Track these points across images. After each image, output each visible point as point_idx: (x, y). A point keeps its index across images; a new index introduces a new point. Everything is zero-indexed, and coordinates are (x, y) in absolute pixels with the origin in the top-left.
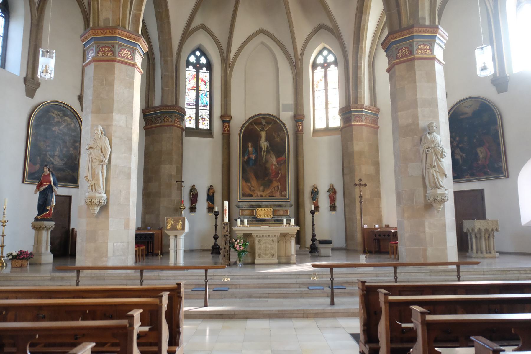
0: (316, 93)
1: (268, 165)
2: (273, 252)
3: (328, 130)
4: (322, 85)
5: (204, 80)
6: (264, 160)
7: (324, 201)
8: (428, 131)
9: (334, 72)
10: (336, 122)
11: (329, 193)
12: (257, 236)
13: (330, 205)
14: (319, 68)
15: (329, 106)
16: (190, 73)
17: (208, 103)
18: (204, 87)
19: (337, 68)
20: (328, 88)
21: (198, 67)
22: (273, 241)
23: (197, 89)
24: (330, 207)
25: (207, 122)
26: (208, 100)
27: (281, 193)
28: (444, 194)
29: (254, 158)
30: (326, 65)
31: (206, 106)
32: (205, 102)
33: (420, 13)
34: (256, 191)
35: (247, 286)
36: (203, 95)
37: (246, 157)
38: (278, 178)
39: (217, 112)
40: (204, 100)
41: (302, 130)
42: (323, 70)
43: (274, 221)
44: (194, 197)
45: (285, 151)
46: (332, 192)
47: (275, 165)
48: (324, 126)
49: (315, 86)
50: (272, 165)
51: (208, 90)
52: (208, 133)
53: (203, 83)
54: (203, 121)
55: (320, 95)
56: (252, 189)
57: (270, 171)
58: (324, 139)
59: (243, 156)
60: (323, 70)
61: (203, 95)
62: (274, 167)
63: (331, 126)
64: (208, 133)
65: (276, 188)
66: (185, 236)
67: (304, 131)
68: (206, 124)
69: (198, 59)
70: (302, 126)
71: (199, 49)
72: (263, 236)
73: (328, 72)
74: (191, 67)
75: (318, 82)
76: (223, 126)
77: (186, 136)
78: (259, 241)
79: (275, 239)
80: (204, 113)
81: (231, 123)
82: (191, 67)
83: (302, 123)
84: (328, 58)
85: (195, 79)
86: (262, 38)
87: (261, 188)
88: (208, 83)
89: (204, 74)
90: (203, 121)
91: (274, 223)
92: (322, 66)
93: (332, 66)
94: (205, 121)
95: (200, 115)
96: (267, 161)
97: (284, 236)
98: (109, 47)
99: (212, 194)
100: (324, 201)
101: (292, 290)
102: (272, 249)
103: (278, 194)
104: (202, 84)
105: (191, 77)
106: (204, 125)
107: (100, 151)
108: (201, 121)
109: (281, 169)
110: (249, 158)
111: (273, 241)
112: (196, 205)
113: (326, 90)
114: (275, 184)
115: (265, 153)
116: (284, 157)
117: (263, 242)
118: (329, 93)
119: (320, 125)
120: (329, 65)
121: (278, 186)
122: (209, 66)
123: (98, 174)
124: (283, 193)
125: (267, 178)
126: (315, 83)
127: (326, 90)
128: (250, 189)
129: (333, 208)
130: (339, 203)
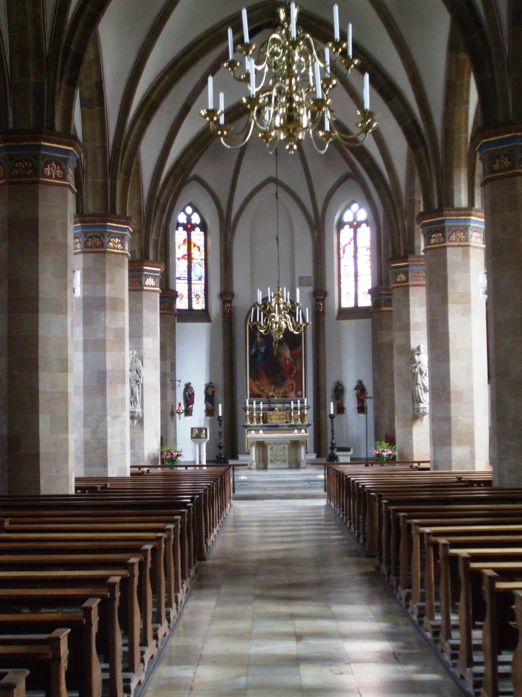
0: (342, 260)
1: (281, 360)
2: (283, 458)
3: (356, 312)
4: (350, 249)
5: (197, 244)
6: (275, 353)
7: (350, 401)
8: (418, 352)
9: (365, 234)
10: (366, 301)
11: (356, 392)
12: (269, 443)
13: (357, 406)
14: (347, 227)
15: (359, 279)
16: (180, 235)
17: (203, 274)
18: (198, 255)
19: (369, 228)
20: (358, 254)
21: (189, 228)
22: (284, 448)
23: (189, 257)
24: (358, 408)
25: (202, 300)
26: (203, 270)
27: (296, 392)
28: (149, 457)
29: (263, 351)
30: (355, 223)
31: (200, 279)
32: (199, 275)
33: (416, 242)
34: (266, 391)
35: (262, 482)
36: (197, 265)
37: (253, 350)
38: (292, 376)
39: (216, 289)
40: (199, 271)
41: (323, 312)
42: (352, 230)
43: (288, 426)
44: (189, 399)
45: (301, 343)
46: (360, 389)
47: (289, 359)
48: (351, 304)
49: (341, 251)
50: (286, 359)
51: (203, 258)
52: (203, 316)
53: (196, 248)
54: (198, 299)
55: (347, 261)
56: (262, 388)
57: (283, 366)
58: (349, 326)
59: (250, 349)
60: (352, 230)
61: (197, 265)
62: (288, 362)
63: (361, 304)
64: (203, 316)
65: (290, 387)
66: (206, 444)
67: (326, 312)
68: (201, 303)
69: (189, 218)
70: (324, 306)
71: (190, 204)
72: (275, 443)
73: (358, 234)
74: (181, 229)
75: (346, 245)
76: (224, 307)
77: (178, 321)
78: (271, 448)
79: (287, 446)
80: (198, 287)
81: (233, 302)
82: (181, 229)
83: (323, 302)
84: (358, 215)
85: (186, 243)
86: (271, 188)
87: (272, 388)
88: (202, 249)
89: (198, 236)
90: (198, 299)
91: (287, 428)
92: (351, 225)
93: (364, 225)
94: (200, 299)
95: (193, 291)
96: (279, 354)
97: (295, 444)
98: (136, 278)
99: (211, 393)
100: (350, 401)
101: (298, 485)
102: (284, 455)
103: (293, 394)
104: (194, 250)
105: (181, 242)
106: (199, 305)
107: (136, 373)
108: (194, 300)
109: (296, 364)
110: (257, 351)
111: (284, 448)
112: (192, 407)
113: (355, 257)
114: (290, 382)
115: (277, 345)
116: (299, 349)
117: (274, 449)
118: (358, 262)
119: (347, 303)
120: (359, 224)
121: (292, 385)
122: (203, 227)
123: (136, 392)
124: (299, 393)
125: (279, 375)
126: (341, 247)
127: (355, 257)
128: (259, 388)
129: (362, 409)
130: (369, 403)
